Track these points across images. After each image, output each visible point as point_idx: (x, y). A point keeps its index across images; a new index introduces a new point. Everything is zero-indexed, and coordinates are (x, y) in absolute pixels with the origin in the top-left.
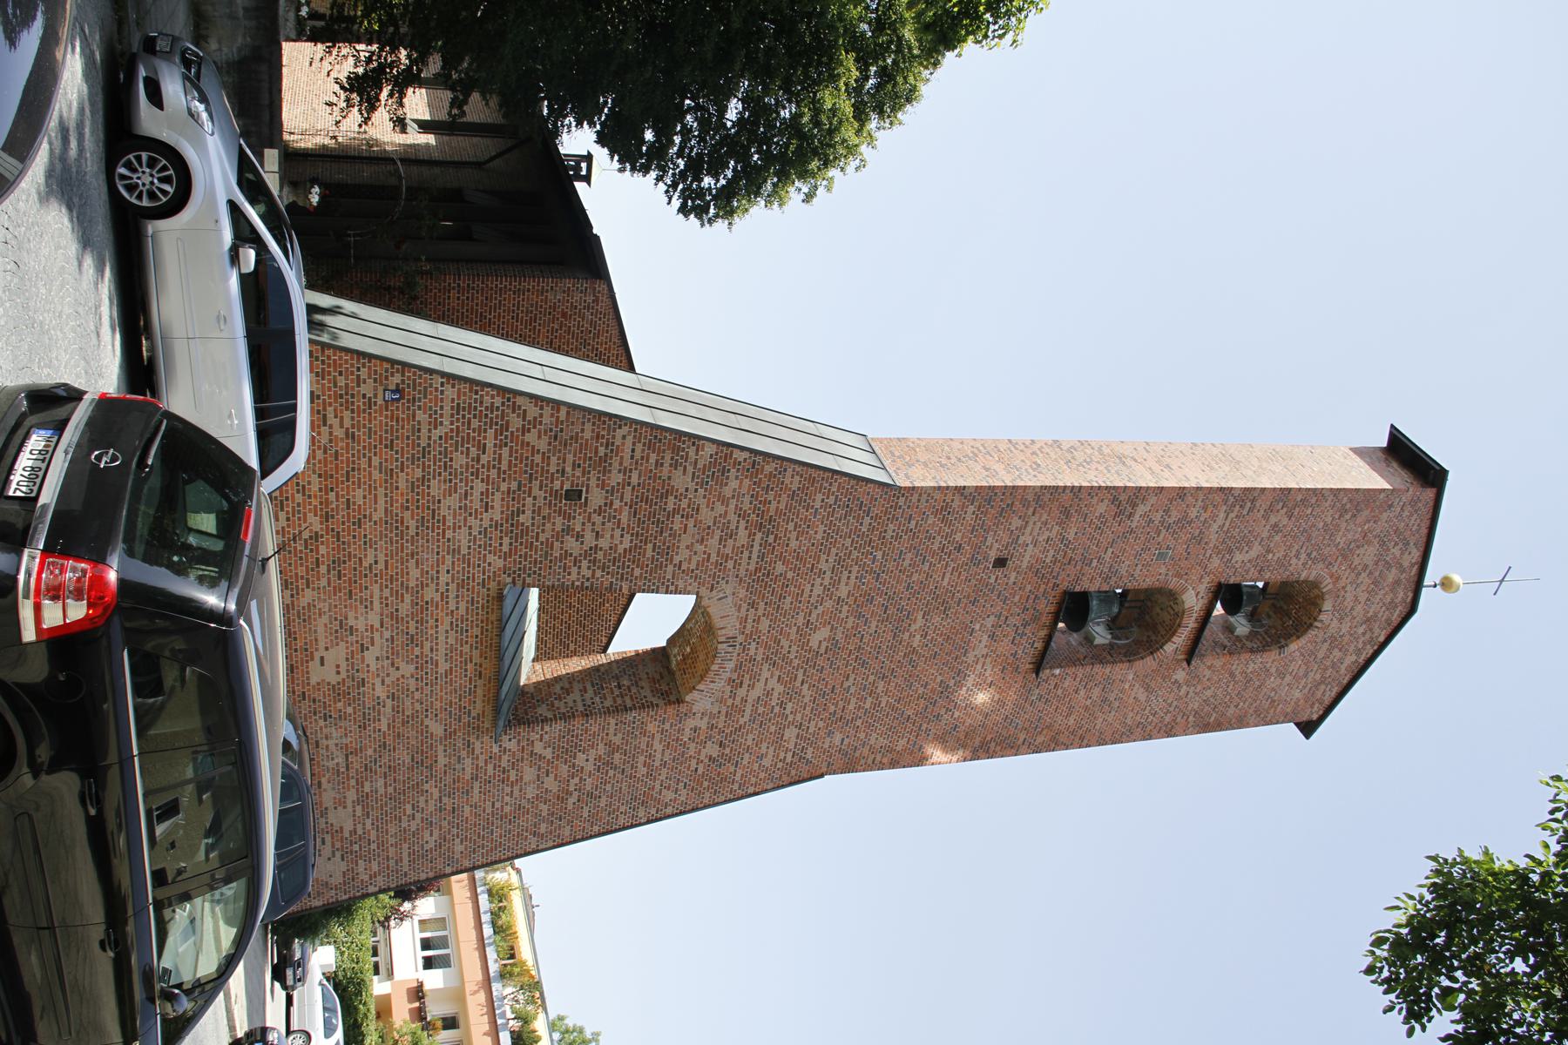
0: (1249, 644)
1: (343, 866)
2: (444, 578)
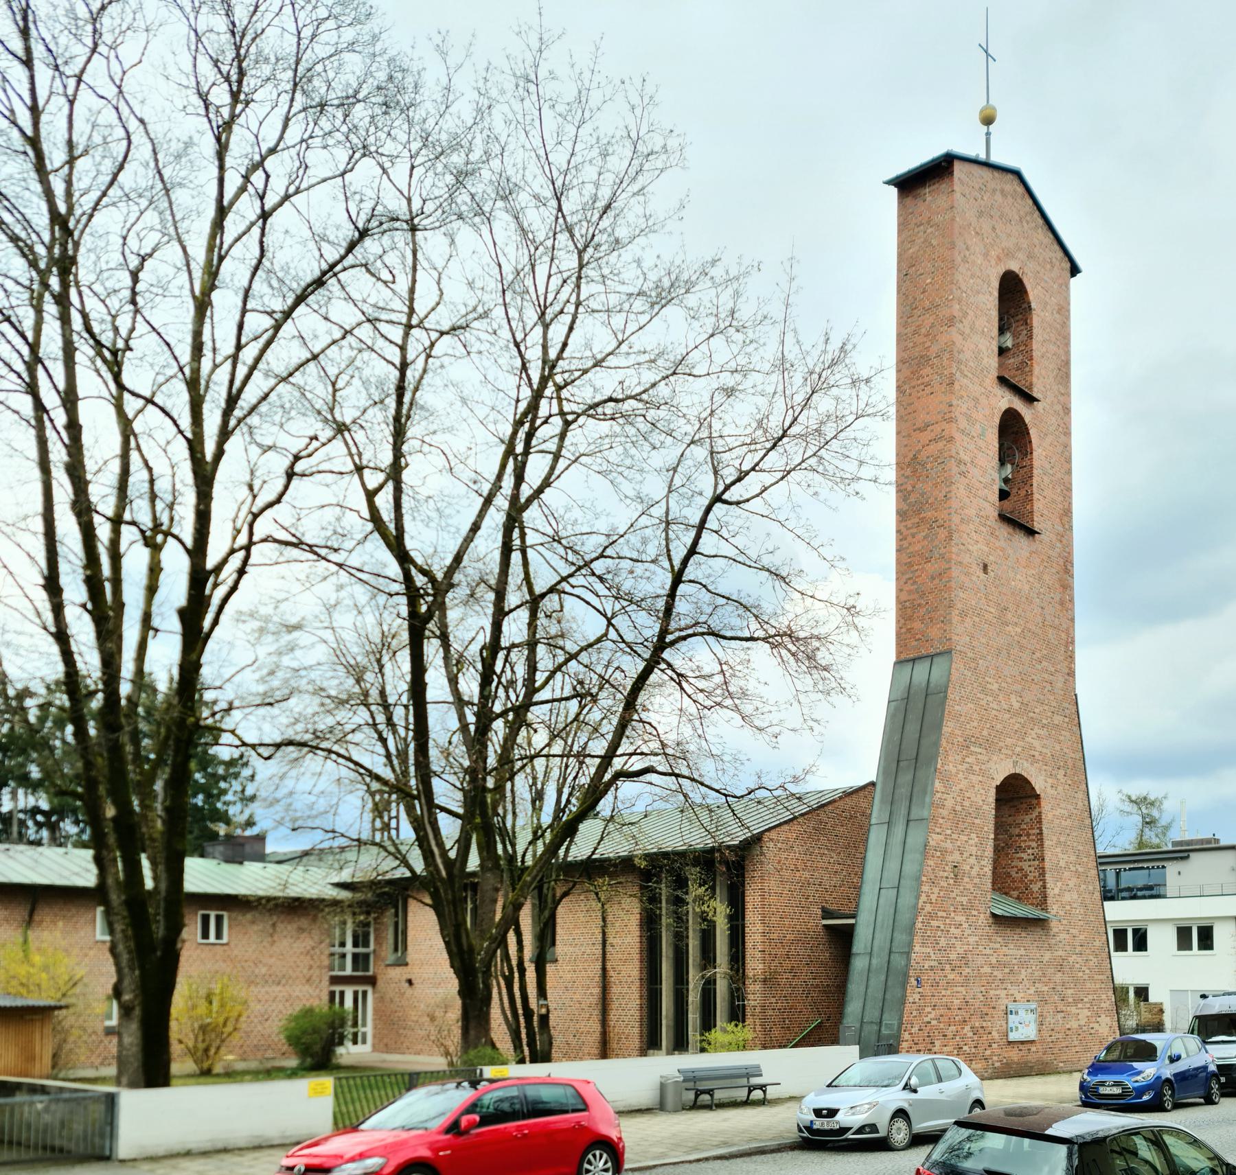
0: (1023, 337)
1: (1103, 1016)
2: (988, 951)
